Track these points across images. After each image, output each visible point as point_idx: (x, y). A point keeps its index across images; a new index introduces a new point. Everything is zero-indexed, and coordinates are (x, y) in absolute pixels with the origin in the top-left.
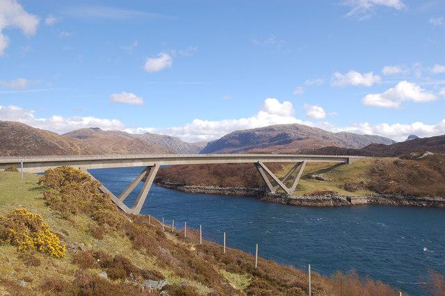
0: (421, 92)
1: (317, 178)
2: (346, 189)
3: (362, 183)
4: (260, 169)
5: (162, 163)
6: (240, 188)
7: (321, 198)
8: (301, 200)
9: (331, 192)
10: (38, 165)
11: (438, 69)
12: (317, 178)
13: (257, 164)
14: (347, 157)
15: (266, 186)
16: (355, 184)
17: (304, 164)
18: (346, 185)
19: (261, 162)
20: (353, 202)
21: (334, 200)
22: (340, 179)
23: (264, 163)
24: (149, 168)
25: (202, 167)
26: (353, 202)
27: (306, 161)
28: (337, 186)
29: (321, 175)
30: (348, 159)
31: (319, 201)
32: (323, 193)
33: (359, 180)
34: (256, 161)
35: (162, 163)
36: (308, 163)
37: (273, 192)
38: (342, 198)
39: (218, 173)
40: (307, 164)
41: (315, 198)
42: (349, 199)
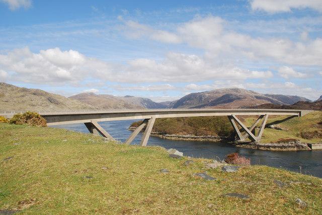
0: (257, 9)
1: (276, 128)
2: (303, 137)
3: (316, 132)
4: (232, 120)
5: (157, 116)
6: (214, 137)
7: (286, 145)
8: (269, 147)
9: (295, 140)
10: (102, 116)
11: (4, 74)
12: (276, 128)
13: (230, 117)
14: (299, 111)
15: (236, 133)
16: (310, 133)
17: (267, 117)
18: (301, 133)
19: (234, 115)
20: (313, 148)
21: (298, 146)
22: (297, 129)
23: (238, 116)
24: (146, 121)
25: (178, 119)
26: (313, 148)
27: (268, 114)
28: (294, 134)
29: (278, 125)
30: (300, 112)
31: (285, 147)
32: (287, 141)
33: (312, 130)
34: (230, 114)
35: (157, 116)
36: (269, 115)
37: (242, 139)
38: (303, 145)
39: (194, 124)
40: (270, 117)
41: (281, 144)
42: (310, 146)
